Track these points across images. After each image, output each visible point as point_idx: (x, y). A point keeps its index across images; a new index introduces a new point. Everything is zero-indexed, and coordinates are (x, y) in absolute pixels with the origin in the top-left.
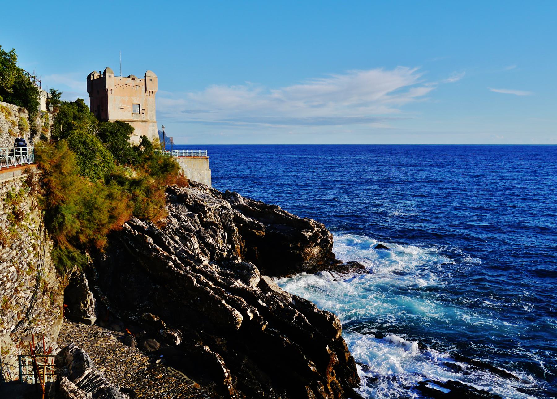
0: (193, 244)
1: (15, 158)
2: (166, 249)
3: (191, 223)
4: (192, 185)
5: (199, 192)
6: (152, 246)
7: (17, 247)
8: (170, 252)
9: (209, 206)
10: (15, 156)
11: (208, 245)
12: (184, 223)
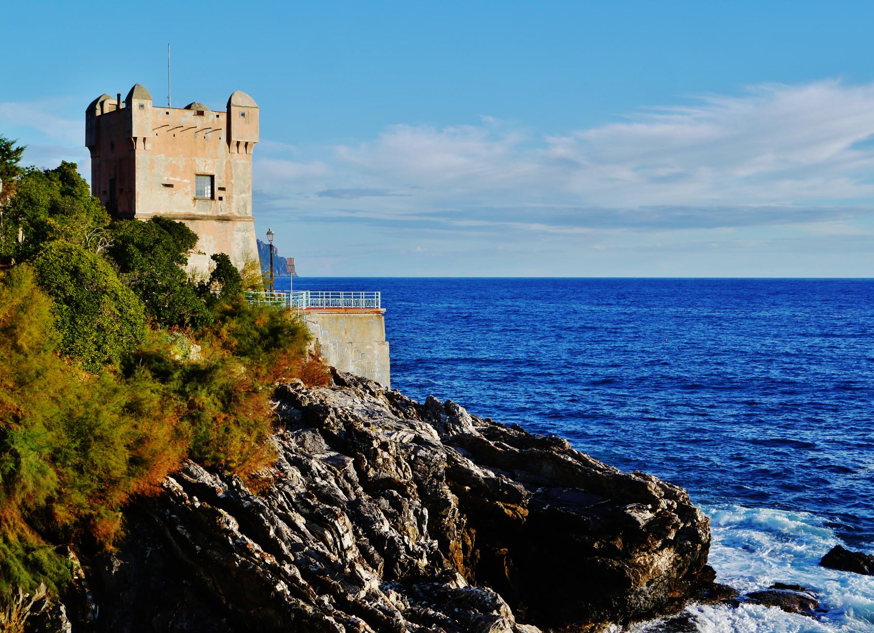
0: (340, 537)
2: (270, 546)
3: (337, 482)
5: (358, 400)
6: (235, 538)
9: (383, 438)
11: (378, 540)
12: (318, 480)
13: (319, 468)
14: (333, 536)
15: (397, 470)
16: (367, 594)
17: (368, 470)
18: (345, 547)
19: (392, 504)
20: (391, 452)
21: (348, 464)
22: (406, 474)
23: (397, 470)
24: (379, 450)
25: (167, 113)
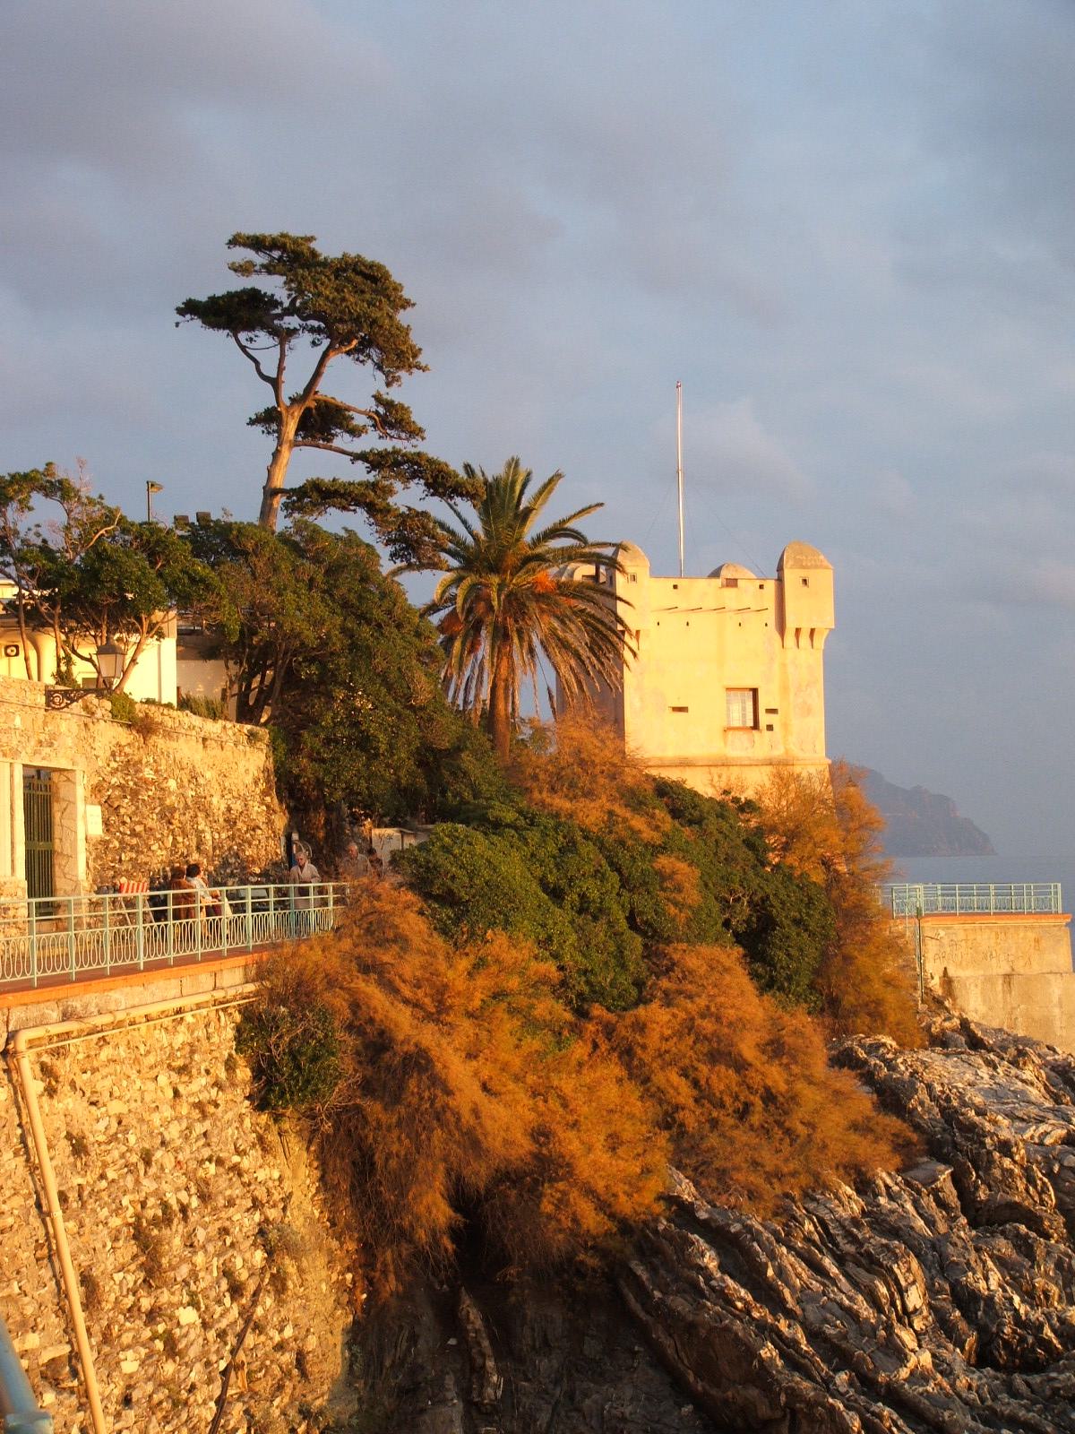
0: (902, 1292)
1: (250, 923)
2: (767, 1294)
3: (916, 1203)
4: (975, 1044)
5: (984, 1072)
6: (709, 1278)
7: (209, 1240)
8: (777, 1305)
9: (1005, 1134)
10: (249, 914)
11: (967, 1299)
12: (883, 1200)
13: (889, 1181)
14: (889, 1290)
15: (1027, 1190)
16: (912, 1373)
17: (977, 1188)
18: (911, 1307)
19: (1017, 1247)
20: (1017, 1158)
21: (942, 1178)
22: (1045, 1197)
23: (1027, 1190)
24: (997, 1155)
25: (675, 587)
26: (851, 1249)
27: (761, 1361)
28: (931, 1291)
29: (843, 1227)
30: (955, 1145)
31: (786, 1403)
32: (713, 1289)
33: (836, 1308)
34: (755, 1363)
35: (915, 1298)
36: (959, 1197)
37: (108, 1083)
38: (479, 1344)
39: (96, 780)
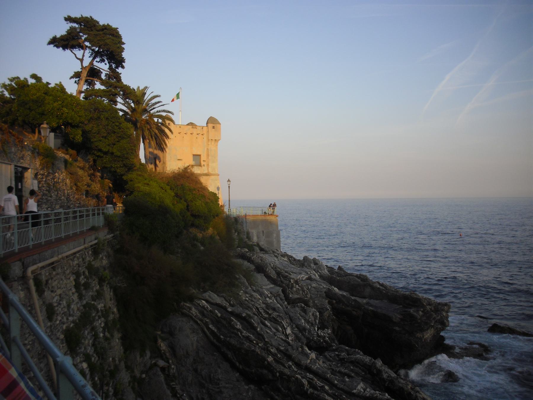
0: (285, 329)
17: (289, 294)
18: (288, 333)
26: (266, 316)
27: (268, 362)
28: (292, 329)
29: (264, 310)
30: (282, 282)
31: (279, 376)
32: (243, 336)
33: (280, 340)
34: (266, 362)
35: (289, 331)
36: (284, 296)
37: (56, 282)
38: (166, 355)
39: (36, 172)
